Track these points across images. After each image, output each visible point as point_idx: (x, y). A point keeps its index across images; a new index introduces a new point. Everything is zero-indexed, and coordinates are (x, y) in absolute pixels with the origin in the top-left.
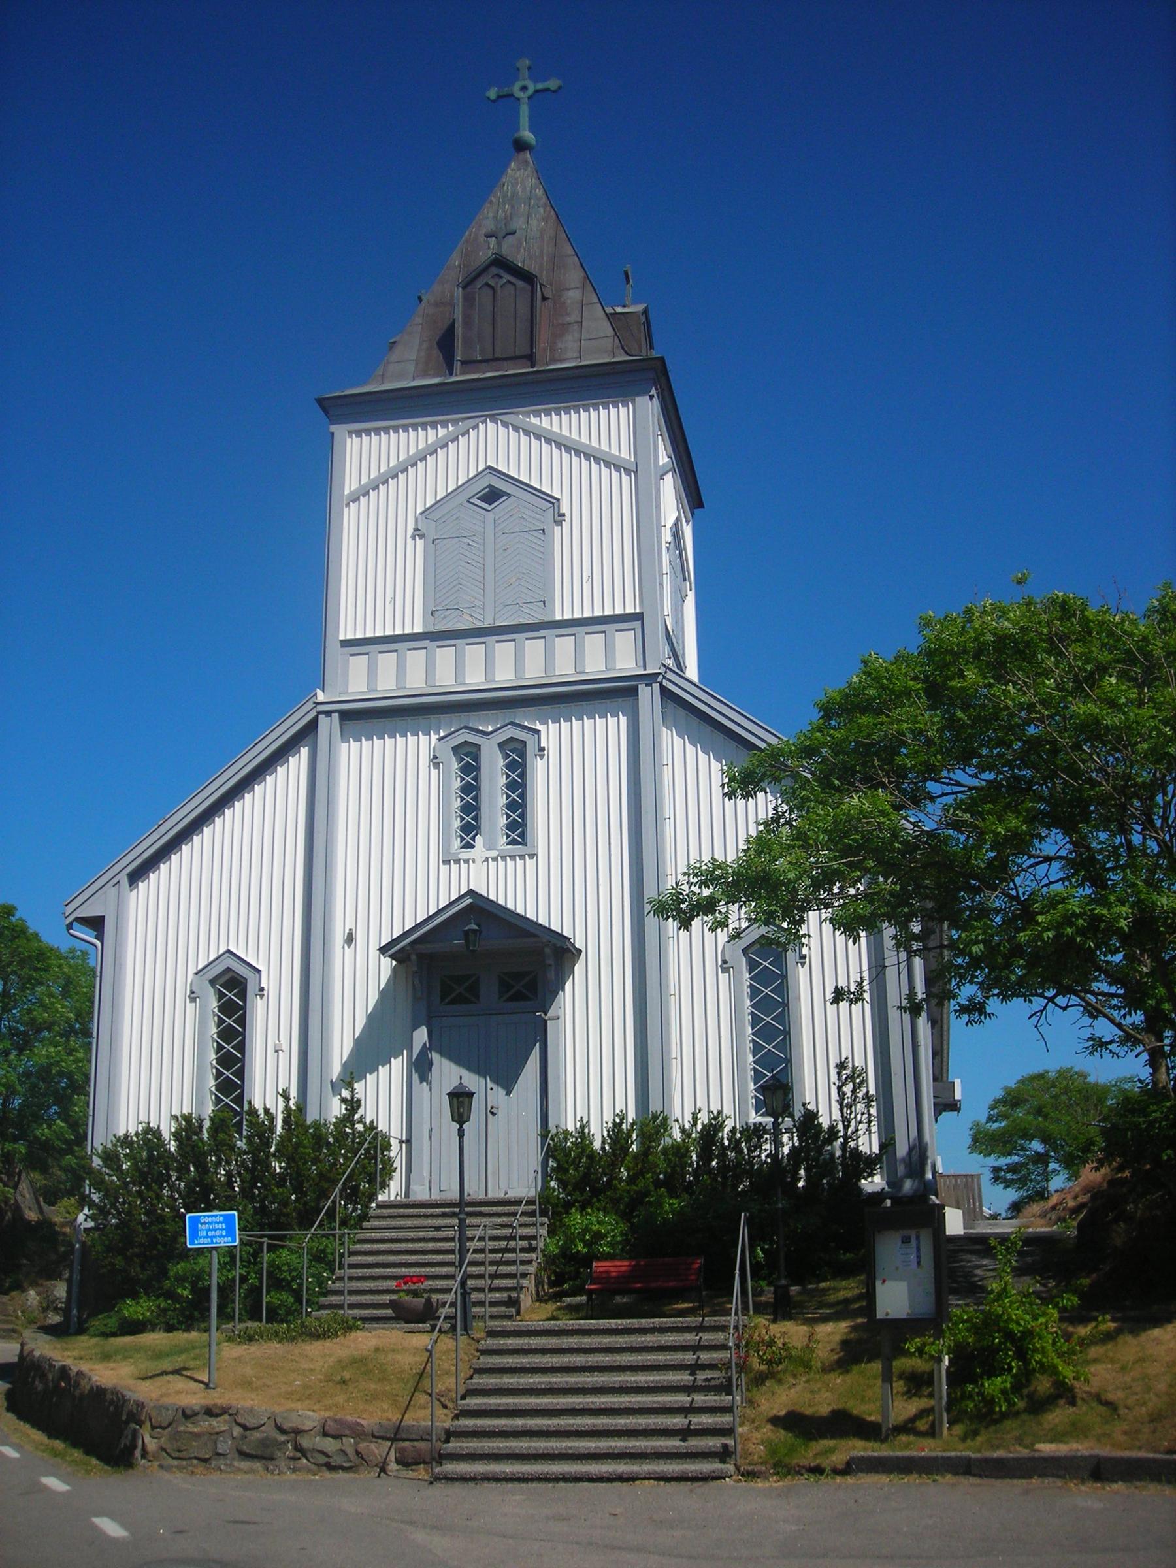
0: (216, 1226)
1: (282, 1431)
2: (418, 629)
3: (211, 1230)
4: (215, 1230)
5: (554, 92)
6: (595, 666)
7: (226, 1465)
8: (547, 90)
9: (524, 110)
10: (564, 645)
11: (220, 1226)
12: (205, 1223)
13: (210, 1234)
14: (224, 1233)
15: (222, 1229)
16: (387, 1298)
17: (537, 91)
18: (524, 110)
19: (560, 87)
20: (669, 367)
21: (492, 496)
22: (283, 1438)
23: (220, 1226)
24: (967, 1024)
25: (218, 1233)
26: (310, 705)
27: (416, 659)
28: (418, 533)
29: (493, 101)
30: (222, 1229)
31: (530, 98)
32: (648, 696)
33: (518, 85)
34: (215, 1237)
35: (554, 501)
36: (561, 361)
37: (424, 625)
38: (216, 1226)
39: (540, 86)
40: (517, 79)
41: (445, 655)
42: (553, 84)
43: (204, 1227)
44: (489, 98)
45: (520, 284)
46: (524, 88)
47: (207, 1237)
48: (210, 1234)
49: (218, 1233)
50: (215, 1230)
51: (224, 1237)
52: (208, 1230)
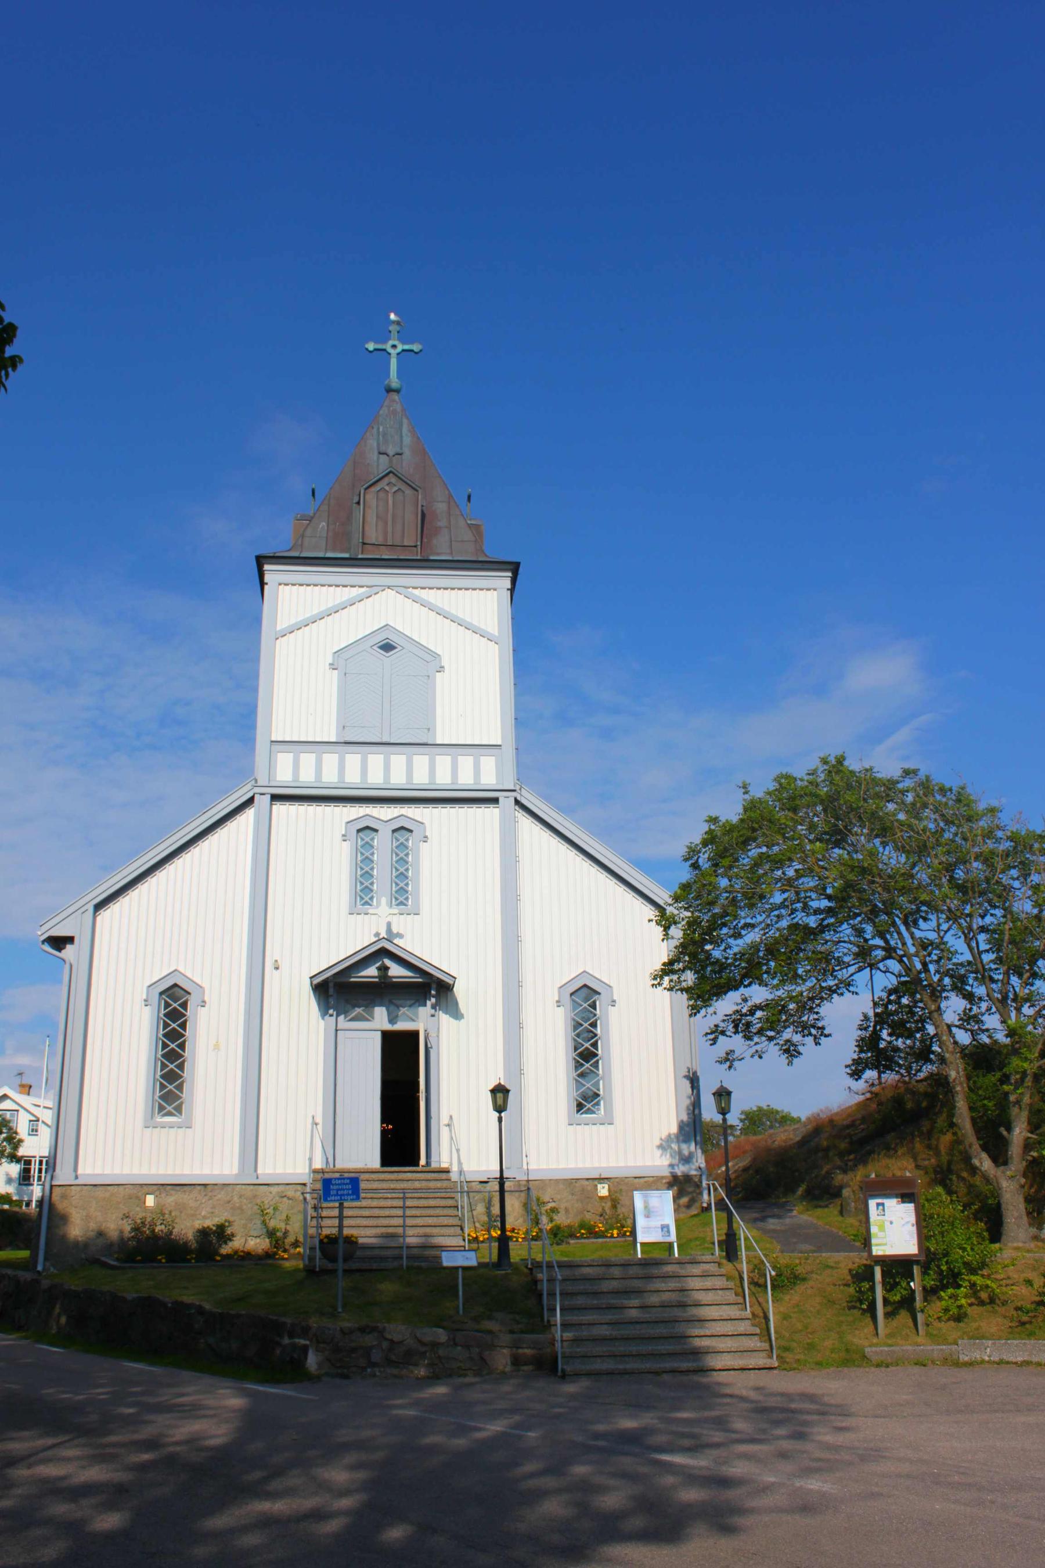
0: (344, 1187)
1: (423, 1344)
2: (333, 739)
3: (341, 1190)
4: (344, 1190)
5: (416, 353)
6: (466, 778)
7: (380, 1371)
8: (412, 351)
9: (394, 362)
10: (443, 762)
11: (347, 1187)
12: (336, 1184)
13: (339, 1193)
14: (350, 1192)
15: (349, 1189)
16: (364, 1203)
17: (403, 350)
18: (394, 362)
19: (421, 351)
20: (521, 570)
21: (387, 647)
22: (423, 1349)
23: (347, 1187)
24: (817, 1044)
25: (346, 1192)
26: (249, 787)
27: (331, 760)
28: (333, 667)
29: (370, 352)
30: (349, 1189)
31: (398, 354)
32: (507, 802)
33: (391, 343)
34: (343, 1195)
35: (436, 656)
36: (438, 554)
37: (337, 734)
38: (344, 1187)
39: (407, 347)
40: (390, 339)
41: (353, 759)
42: (416, 347)
43: (335, 1187)
44: (367, 349)
45: (408, 492)
46: (394, 346)
47: (337, 1195)
48: (339, 1193)
49: (346, 1192)
50: (344, 1190)
51: (350, 1195)
52: (338, 1190)
